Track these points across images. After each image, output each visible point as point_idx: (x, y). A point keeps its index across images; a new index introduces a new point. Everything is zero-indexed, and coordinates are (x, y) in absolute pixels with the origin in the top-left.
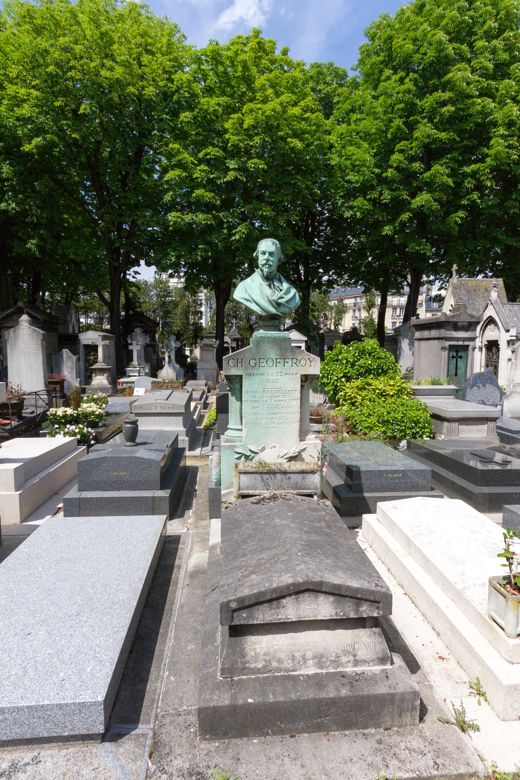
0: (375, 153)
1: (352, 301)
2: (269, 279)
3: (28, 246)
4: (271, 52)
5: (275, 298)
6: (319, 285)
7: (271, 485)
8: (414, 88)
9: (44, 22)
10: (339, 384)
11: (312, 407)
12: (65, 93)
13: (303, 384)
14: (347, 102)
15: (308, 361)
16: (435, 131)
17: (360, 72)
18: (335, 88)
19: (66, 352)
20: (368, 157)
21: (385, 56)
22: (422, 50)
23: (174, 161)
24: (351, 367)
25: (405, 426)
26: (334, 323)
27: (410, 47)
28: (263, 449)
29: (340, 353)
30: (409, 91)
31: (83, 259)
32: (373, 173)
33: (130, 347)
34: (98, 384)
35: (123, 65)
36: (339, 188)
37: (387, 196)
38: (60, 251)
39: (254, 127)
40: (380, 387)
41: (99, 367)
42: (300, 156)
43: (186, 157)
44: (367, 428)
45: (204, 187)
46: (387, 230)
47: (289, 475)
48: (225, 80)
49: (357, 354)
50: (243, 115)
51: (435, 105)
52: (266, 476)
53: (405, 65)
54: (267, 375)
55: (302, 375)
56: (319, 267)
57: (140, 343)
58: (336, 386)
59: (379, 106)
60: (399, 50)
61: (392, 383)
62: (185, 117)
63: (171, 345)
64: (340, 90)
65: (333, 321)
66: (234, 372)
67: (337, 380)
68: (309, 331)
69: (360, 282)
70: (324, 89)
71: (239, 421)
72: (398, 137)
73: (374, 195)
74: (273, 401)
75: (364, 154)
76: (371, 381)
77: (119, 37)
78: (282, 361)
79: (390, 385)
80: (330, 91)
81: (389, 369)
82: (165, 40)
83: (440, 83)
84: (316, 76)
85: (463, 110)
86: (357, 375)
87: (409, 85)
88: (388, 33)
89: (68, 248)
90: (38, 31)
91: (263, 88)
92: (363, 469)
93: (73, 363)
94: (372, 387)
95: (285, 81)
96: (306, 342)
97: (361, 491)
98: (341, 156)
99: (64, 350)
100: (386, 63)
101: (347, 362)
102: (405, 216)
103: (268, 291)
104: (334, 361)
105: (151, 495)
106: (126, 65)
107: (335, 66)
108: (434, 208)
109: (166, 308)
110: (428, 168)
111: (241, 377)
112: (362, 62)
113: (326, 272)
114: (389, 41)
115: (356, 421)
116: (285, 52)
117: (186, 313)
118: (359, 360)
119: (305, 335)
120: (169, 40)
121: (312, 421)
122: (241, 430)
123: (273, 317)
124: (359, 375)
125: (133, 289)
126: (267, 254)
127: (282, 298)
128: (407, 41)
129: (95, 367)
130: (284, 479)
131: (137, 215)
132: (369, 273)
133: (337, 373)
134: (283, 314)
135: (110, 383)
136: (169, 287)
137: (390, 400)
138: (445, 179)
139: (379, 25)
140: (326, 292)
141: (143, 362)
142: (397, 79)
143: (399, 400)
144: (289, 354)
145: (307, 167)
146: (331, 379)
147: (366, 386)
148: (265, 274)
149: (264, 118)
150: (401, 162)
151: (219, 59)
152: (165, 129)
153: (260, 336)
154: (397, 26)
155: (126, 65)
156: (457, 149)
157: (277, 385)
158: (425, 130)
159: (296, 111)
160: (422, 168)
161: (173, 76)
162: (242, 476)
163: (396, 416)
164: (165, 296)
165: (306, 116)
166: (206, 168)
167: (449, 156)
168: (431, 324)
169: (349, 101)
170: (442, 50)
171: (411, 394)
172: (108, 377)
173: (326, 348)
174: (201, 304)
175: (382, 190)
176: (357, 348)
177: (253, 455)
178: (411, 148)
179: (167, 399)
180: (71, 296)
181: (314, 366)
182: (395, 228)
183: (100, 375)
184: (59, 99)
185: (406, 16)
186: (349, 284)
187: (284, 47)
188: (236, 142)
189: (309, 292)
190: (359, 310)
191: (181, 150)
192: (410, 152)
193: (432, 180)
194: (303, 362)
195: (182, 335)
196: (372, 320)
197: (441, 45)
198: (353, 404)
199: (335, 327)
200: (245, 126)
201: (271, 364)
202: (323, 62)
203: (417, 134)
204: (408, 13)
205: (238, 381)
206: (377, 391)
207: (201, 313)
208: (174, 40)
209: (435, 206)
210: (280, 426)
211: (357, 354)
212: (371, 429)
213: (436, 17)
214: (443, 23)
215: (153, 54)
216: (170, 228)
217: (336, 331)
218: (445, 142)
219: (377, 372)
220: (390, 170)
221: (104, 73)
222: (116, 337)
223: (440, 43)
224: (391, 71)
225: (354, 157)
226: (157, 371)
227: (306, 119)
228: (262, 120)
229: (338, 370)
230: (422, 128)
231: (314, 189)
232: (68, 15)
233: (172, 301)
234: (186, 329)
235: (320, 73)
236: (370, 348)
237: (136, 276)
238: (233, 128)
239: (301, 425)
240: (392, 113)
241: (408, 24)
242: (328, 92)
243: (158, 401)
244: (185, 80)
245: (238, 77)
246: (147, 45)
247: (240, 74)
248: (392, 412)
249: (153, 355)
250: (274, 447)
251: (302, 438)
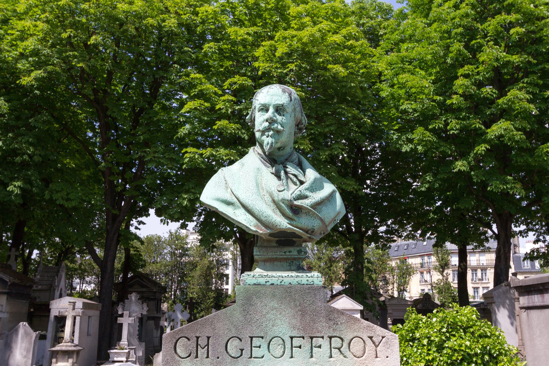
2: (274, 159)
3: (10, 188)
5: (288, 195)
6: (375, 238)
12: (75, 25)
14: (395, 33)
15: (368, 341)
16: (505, 54)
17: (407, 4)
19: (24, 327)
23: (194, 92)
26: (398, 288)
29: (417, 328)
30: (467, 15)
31: (74, 204)
32: (434, 101)
36: (393, 120)
37: (454, 126)
38: (47, 197)
39: (289, 55)
41: (64, 348)
42: (344, 84)
43: (209, 87)
46: (460, 165)
49: (444, 330)
51: (500, 29)
56: (373, 215)
59: (434, 32)
62: (208, 47)
63: (177, 317)
65: (396, 285)
68: (365, 298)
70: (368, 22)
72: (460, 62)
73: (438, 124)
75: (422, 81)
81: (501, 354)
84: (358, 11)
85: (533, 32)
89: (57, 192)
91: (299, 16)
93: (30, 343)
101: (430, 342)
102: (481, 148)
108: (517, 138)
110: (502, 94)
113: (383, 222)
117: (207, 276)
118: (448, 339)
119: (361, 303)
123: (284, 240)
125: (136, 243)
126: (271, 110)
127: (306, 197)
129: (57, 348)
131: (145, 152)
132: (439, 221)
136: (187, 243)
138: (526, 105)
140: (385, 247)
141: (135, 341)
142: (451, 6)
144: (322, 327)
145: (354, 96)
149: (300, 45)
150: (467, 87)
152: (187, 62)
153: (254, 281)
156: (534, 73)
158: (491, 53)
159: (338, 38)
160: (495, 93)
164: (181, 256)
166: (231, 98)
167: (526, 80)
168: (543, 284)
169: (397, 32)
175: (447, 119)
176: (443, 320)
178: (478, 73)
180: (65, 253)
182: (469, 163)
184: (67, 30)
186: (413, 237)
188: (268, 69)
190: (429, 272)
191: (203, 80)
192: (477, 77)
193: (511, 106)
194: (357, 346)
195: (198, 304)
196: (447, 284)
199: (399, 294)
200: (278, 54)
201: (278, 351)
203: (482, 57)
207: (227, 276)
209: (519, 136)
216: (184, 166)
218: (519, 65)
220: (455, 96)
228: (298, 47)
230: (488, 50)
233: (189, 263)
234: (205, 296)
236: (465, 319)
237: (139, 227)
238: (264, 56)
240: (449, 38)
245: (270, 9)
249: (155, 331)
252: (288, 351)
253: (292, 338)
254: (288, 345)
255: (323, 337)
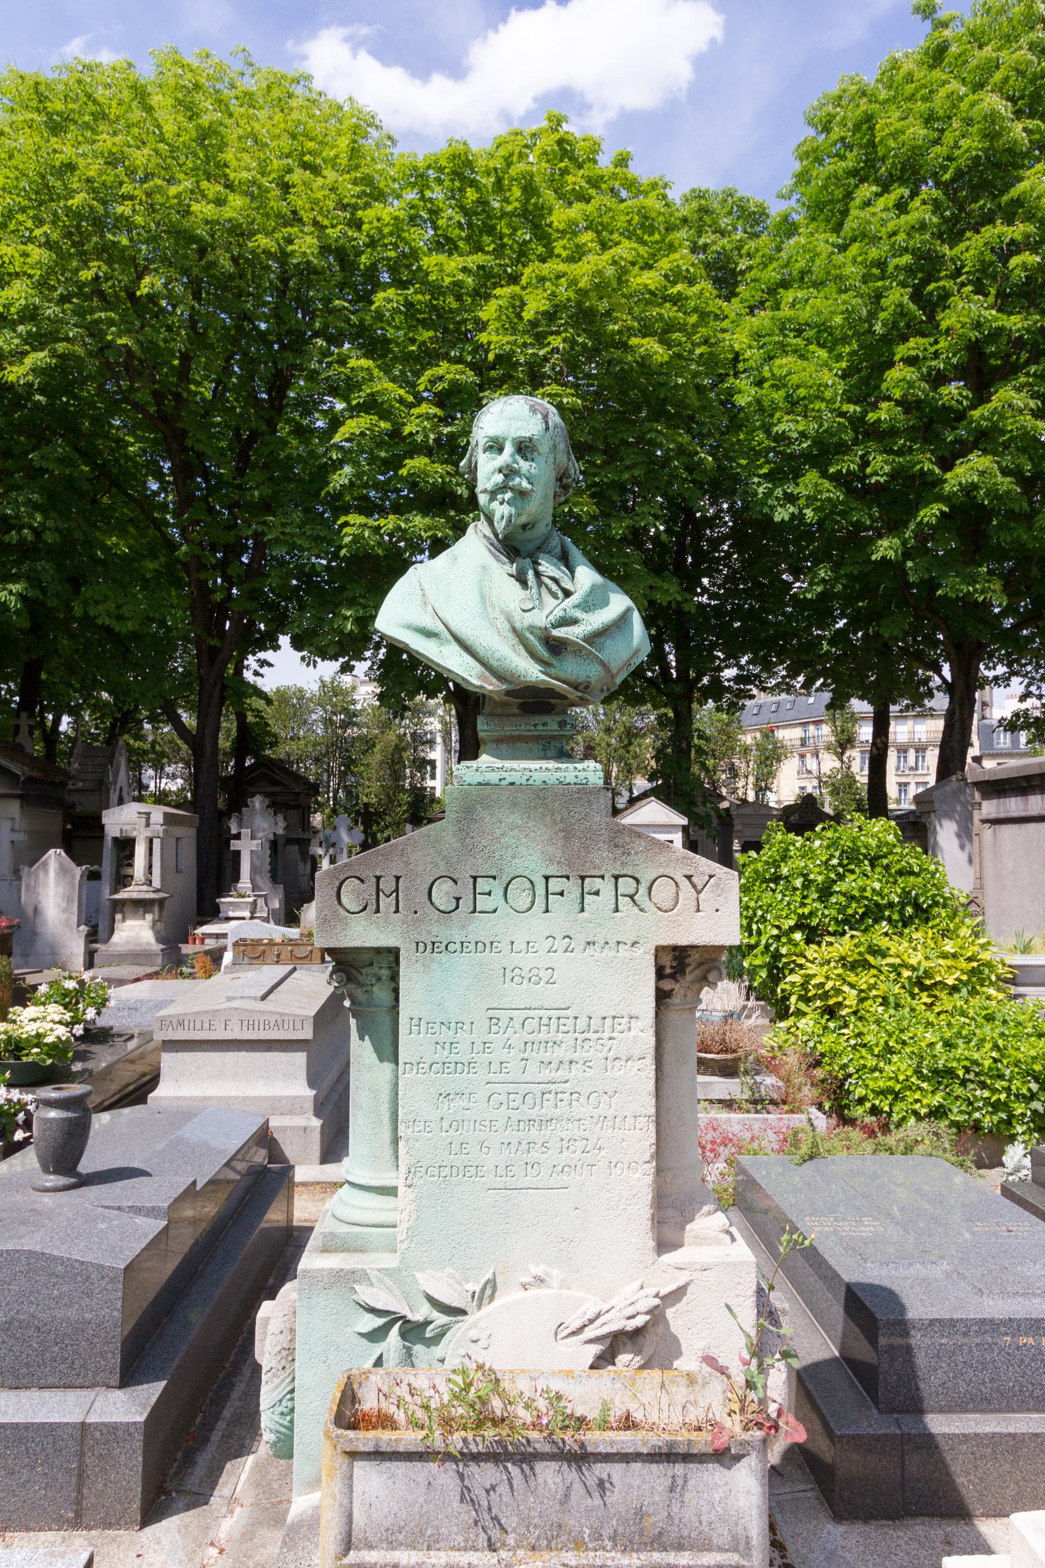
0: (844, 370)
1: (797, 733)
2: (516, 548)
4: (590, 160)
5: (540, 618)
6: (716, 690)
7: (510, 1521)
8: (935, 220)
9: (70, 106)
10: (784, 951)
11: (707, 1022)
12: (109, 253)
13: (667, 985)
14: (771, 267)
15: (685, 884)
17: (798, 201)
18: (740, 241)
19: (55, 857)
20: (827, 377)
21: (857, 157)
22: (949, 138)
24: (820, 899)
25: (1008, 1090)
27: (917, 131)
28: (489, 1291)
30: (923, 226)
32: (842, 414)
33: (235, 845)
34: (127, 943)
35: (246, 193)
36: (758, 454)
37: (881, 467)
39: (550, 316)
40: (913, 962)
41: (135, 896)
42: (662, 379)
44: (882, 1093)
45: (429, 452)
46: (886, 548)
47: (600, 1470)
48: (480, 225)
49: (835, 862)
50: (524, 288)
51: (989, 257)
52: (484, 1474)
53: (910, 172)
54: (505, 946)
55: (659, 950)
56: (713, 646)
57: (260, 835)
58: (777, 956)
60: (892, 144)
61: (949, 947)
62: (385, 299)
63: (341, 839)
64: (752, 245)
65: (751, 779)
66: (363, 933)
67: (777, 938)
69: (818, 683)
70: (714, 243)
71: (388, 1151)
73: (848, 464)
74: (532, 1067)
75: (820, 372)
76: (884, 943)
77: (240, 138)
78: (572, 888)
79: (944, 956)
80: (729, 247)
81: (936, 904)
82: (344, 143)
83: (999, 205)
84: (696, 216)
86: (838, 922)
87: (919, 212)
88: (863, 108)
90: (56, 127)
91: (571, 230)
92: (916, 1310)
94: (889, 960)
95: (624, 218)
96: (685, 829)
97: (915, 1407)
98: (760, 383)
99: (52, 851)
100: (861, 175)
101: (807, 884)
102: (930, 513)
103: (510, 594)
104: (770, 880)
105: (75, 1417)
106: (254, 193)
107: (739, 194)
109: (344, 752)
110: (981, 396)
111: (394, 953)
112: (803, 178)
113: (732, 656)
114: (865, 127)
115: (844, 1067)
116: (622, 161)
117: (394, 764)
118: (841, 877)
119: (683, 812)
120: (354, 141)
121: (705, 1066)
122: (390, 1191)
123: (534, 701)
124: (845, 921)
125: (259, 704)
126: (509, 449)
127: (575, 622)
128: (911, 119)
130: (578, 1489)
131: (265, 523)
133: (778, 917)
134: (576, 687)
135: (159, 940)
136: (354, 702)
137: (947, 1002)
139: (840, 97)
140: (733, 708)
141: (265, 883)
143: (975, 1001)
144: (603, 858)
145: (681, 405)
146: (759, 933)
147: (870, 958)
148: (500, 526)
149: (572, 295)
150: (911, 385)
151: (467, 173)
154: (883, 95)
155: (254, 193)
157: (553, 996)
158: (966, 312)
159: (650, 279)
160: (966, 397)
161: (360, 213)
162: (361, 1468)
163: (976, 1056)
164: (345, 725)
165: (674, 290)
168: (1028, 778)
169: (775, 264)
170: (997, 135)
171: (1006, 981)
172: (154, 922)
173: (736, 846)
174: (431, 743)
175: (867, 453)
176: (834, 844)
177: (441, 1319)
178: (936, 355)
179: (264, 998)
181: (713, 910)
182: (904, 543)
183: (135, 916)
184: (91, 264)
185: (902, 72)
186: (789, 689)
187: (618, 151)
188: (507, 348)
189: (690, 709)
190: (816, 754)
191: (376, 372)
192: (934, 363)
194: (663, 891)
196: (850, 778)
197: (993, 122)
198: (831, 1012)
199: (757, 795)
200: (528, 315)
202: (712, 188)
203: (947, 320)
204: (908, 66)
205: (385, 973)
206: (906, 973)
207: (432, 763)
208: (369, 144)
209: (1006, 484)
210: (564, 1179)
211: (835, 862)
212: (897, 1096)
213: (978, 67)
214: (998, 76)
215: (315, 170)
216: (343, 552)
217: (760, 805)
219: (901, 913)
220: (884, 405)
221: (202, 209)
222: (201, 821)
223: (992, 117)
224: (874, 188)
225: (794, 379)
226: (298, 909)
227: (677, 300)
229: (783, 908)
230: (961, 304)
231: (697, 453)
232: (127, 95)
233: (360, 738)
234: (391, 801)
235: (704, 211)
236: (873, 843)
237: (261, 671)
239: (659, 1171)
240: (882, 278)
241: (909, 88)
242: (723, 248)
243: (235, 1004)
244: (387, 219)
245: (512, 214)
246: (303, 154)
247: (517, 204)
248: (960, 1042)
249: (301, 865)
250: (540, 1281)
251: (669, 1234)
252: (540, 901)
253: (547, 878)
254: (540, 891)
255: (602, 877)
